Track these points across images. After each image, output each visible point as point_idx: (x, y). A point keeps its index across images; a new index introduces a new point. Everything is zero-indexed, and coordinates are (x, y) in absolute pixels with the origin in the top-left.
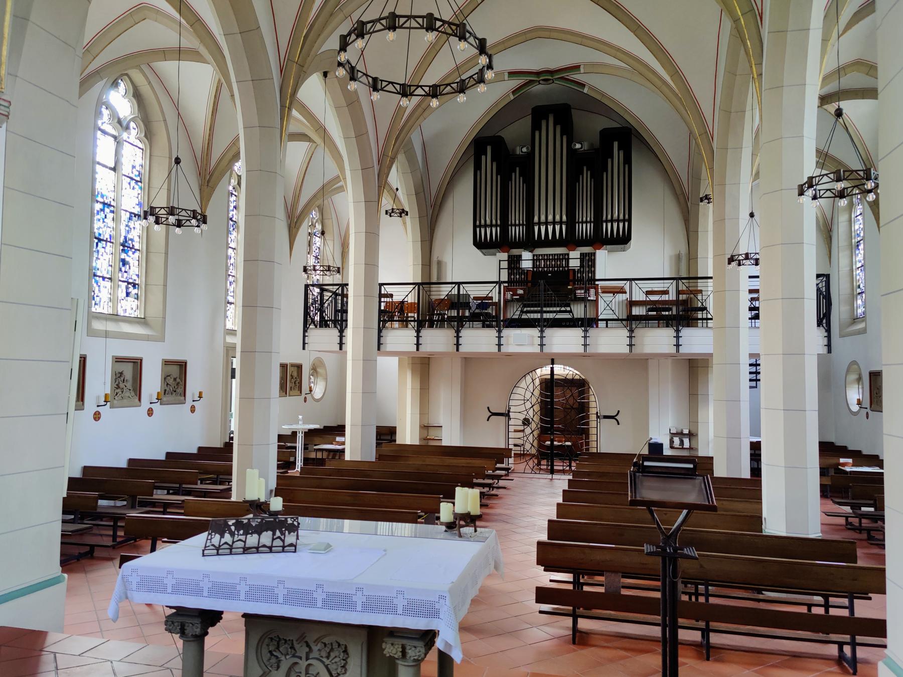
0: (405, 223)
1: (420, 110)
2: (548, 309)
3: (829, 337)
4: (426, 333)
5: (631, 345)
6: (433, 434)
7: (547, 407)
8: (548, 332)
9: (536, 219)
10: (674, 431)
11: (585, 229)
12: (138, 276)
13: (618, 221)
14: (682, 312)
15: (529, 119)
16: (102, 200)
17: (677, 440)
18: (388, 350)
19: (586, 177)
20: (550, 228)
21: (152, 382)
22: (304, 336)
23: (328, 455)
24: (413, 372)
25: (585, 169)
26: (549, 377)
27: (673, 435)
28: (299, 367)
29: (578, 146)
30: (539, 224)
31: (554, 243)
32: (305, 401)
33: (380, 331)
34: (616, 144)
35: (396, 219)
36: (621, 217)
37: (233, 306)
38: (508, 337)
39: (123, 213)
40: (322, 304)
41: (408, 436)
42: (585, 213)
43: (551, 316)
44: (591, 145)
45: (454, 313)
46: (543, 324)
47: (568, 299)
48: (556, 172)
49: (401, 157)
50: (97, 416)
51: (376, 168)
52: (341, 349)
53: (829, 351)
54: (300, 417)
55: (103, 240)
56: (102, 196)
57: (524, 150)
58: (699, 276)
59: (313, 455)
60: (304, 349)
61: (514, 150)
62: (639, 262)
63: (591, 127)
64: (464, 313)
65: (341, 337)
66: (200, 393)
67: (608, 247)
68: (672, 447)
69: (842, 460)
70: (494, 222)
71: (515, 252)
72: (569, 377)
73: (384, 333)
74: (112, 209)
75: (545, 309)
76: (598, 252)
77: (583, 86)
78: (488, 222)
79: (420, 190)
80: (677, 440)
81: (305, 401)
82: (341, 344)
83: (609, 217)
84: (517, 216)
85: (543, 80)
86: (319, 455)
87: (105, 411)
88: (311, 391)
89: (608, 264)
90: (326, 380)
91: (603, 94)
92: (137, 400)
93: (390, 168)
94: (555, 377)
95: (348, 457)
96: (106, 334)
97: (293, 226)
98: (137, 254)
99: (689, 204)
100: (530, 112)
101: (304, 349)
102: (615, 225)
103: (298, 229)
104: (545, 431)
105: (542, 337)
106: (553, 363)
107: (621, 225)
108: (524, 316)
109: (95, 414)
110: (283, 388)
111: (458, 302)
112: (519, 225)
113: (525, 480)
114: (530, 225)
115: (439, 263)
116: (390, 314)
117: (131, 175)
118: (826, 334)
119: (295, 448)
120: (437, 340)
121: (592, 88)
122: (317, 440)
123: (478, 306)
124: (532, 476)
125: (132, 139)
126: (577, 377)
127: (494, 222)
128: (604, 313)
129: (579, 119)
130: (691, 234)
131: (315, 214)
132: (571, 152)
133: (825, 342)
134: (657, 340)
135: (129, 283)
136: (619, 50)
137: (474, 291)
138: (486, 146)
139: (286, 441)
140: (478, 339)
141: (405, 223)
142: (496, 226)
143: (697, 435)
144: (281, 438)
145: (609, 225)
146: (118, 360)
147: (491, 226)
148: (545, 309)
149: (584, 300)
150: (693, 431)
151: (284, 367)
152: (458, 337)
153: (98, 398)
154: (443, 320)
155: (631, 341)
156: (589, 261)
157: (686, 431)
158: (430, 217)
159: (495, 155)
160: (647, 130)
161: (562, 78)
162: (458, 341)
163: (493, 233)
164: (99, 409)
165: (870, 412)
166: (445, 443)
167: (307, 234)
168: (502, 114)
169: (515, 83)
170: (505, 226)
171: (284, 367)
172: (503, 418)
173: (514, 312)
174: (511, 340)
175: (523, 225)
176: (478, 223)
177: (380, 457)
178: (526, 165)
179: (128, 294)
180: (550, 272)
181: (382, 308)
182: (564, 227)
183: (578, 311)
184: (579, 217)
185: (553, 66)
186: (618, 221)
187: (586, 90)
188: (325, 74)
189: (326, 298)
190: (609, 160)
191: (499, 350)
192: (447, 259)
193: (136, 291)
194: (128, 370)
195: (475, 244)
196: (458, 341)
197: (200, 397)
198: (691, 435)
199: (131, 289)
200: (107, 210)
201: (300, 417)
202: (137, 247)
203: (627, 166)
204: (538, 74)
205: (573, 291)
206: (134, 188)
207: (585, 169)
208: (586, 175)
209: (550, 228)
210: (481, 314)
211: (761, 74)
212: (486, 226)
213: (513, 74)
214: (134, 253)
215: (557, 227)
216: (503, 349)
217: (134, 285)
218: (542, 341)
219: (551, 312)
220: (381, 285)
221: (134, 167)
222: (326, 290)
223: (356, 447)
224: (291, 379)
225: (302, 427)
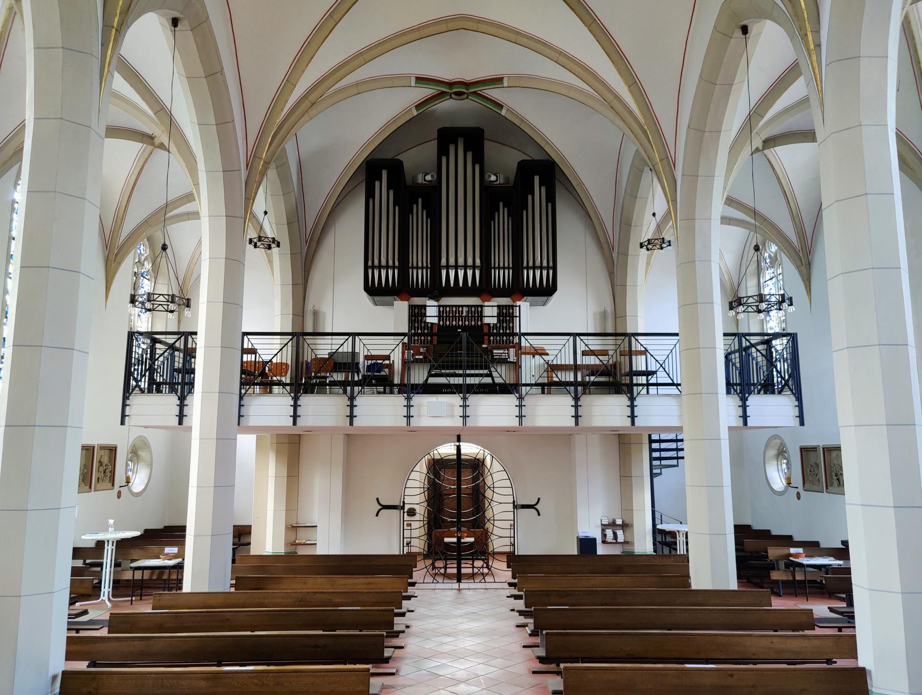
0: (270, 262)
1: (306, 104)
2: (472, 372)
3: (800, 407)
4: (306, 400)
5: (521, 417)
6: (303, 536)
7: (435, 495)
8: (473, 399)
10: (606, 522)
11: (501, 276)
14: (615, 377)
15: (435, 143)
17: (609, 532)
19: (503, 217)
20: (461, 273)
23: (152, 574)
24: (278, 453)
26: (455, 457)
27: (604, 527)
28: (112, 450)
30: (448, 267)
31: (465, 291)
32: (119, 497)
33: (241, 398)
34: (537, 179)
35: (261, 252)
38: (420, 406)
40: (153, 359)
41: (268, 541)
42: (502, 256)
43: (476, 381)
44: (507, 179)
45: (339, 377)
47: (486, 362)
48: (460, 213)
49: (272, 173)
51: (244, 174)
52: (180, 423)
53: (802, 423)
54: (111, 521)
57: (428, 178)
58: (639, 332)
59: (128, 575)
60: (122, 423)
61: (415, 178)
62: (557, 322)
63: (504, 162)
64: (353, 377)
65: (182, 406)
67: (529, 298)
68: (604, 542)
69: (793, 550)
70: (391, 263)
71: (417, 301)
73: (246, 400)
75: (468, 372)
77: (501, 106)
78: (384, 263)
79: (294, 218)
80: (609, 532)
81: (119, 497)
82: (181, 417)
83: (531, 264)
84: (419, 256)
85: (455, 93)
86: (138, 575)
88: (128, 482)
89: (530, 316)
90: (151, 465)
91: (522, 120)
93: (263, 174)
94: (462, 457)
95: (187, 587)
97: (112, 258)
99: (615, 255)
100: (435, 135)
101: (122, 423)
102: (538, 273)
103: (119, 264)
104: (435, 522)
105: (465, 406)
106: (459, 440)
108: (432, 380)
110: (86, 481)
111: (343, 363)
112: (422, 268)
114: (435, 267)
115: (316, 314)
116: (256, 377)
118: (797, 403)
119: (100, 565)
120: (323, 410)
121: (510, 110)
122: (135, 553)
123: (369, 368)
124: (432, 586)
128: (527, 376)
129: (490, 150)
130: (618, 289)
131: (143, 250)
132: (486, 188)
133: (796, 412)
134: (608, 411)
136: (561, 53)
137: (366, 348)
138: (379, 170)
139: (87, 558)
140: (379, 410)
141: (270, 262)
143: (632, 526)
144: (77, 552)
145: (531, 272)
148: (468, 372)
149: (504, 361)
150: (627, 522)
151: (88, 450)
152: (352, 406)
154: (325, 384)
156: (507, 315)
157: (619, 522)
158: (304, 256)
162: (632, 412)
165: (802, 493)
166: (322, 549)
167: (130, 274)
168: (403, 132)
169: (426, 92)
170: (404, 266)
171: (88, 450)
173: (419, 376)
174: (424, 410)
176: (370, 263)
177: (240, 583)
178: (430, 197)
180: (459, 327)
183: (501, 374)
185: (469, 77)
186: (541, 268)
187: (503, 112)
188: (175, 22)
189: (159, 352)
190: (530, 197)
192: (326, 308)
195: (365, 290)
196: (632, 412)
198: (625, 526)
201: (111, 521)
203: (550, 205)
204: (451, 84)
205: (489, 352)
209: (461, 273)
210: (374, 377)
211: (820, 45)
212: (380, 267)
213: (421, 80)
215: (470, 273)
216: (414, 422)
218: (465, 411)
219: (477, 375)
220: (246, 334)
222: (160, 342)
223: (201, 570)
224: (99, 467)
225: (112, 535)
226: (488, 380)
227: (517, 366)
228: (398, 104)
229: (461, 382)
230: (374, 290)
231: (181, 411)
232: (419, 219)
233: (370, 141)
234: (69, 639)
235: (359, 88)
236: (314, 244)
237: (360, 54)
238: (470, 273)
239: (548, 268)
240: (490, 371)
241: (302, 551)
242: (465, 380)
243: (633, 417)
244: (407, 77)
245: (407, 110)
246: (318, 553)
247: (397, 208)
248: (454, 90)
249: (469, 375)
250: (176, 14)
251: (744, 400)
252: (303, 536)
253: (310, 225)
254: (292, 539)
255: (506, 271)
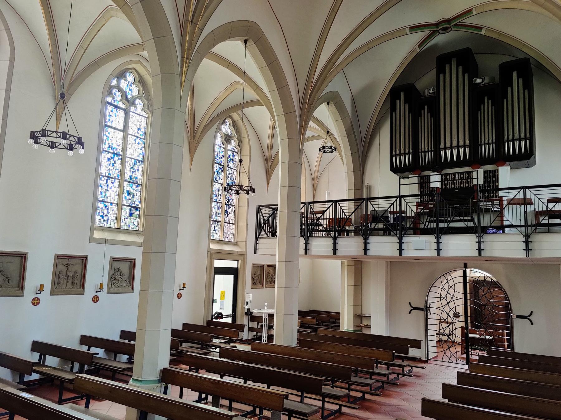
9: (442, 146)
11: (487, 150)
12: (140, 202)
13: (520, 140)
16: (112, 151)
18: (313, 254)
19: (487, 107)
21: (97, 274)
22: (256, 244)
25: (486, 98)
29: (478, 81)
30: (445, 149)
31: (459, 163)
34: (515, 74)
36: (523, 135)
37: (220, 223)
39: (127, 160)
42: (487, 135)
46: (439, 233)
50: (95, 299)
55: (112, 178)
56: (113, 149)
57: (431, 91)
60: (255, 253)
66: (184, 284)
67: (511, 163)
71: (425, 173)
72: (481, 279)
74: (120, 157)
76: (500, 168)
77: (480, 28)
79: (352, 132)
84: (426, 144)
85: (442, 29)
87: (102, 295)
91: (500, 33)
92: (130, 288)
95: (274, 343)
96: (106, 242)
98: (139, 188)
101: (255, 253)
102: (517, 144)
106: (466, 266)
107: (523, 143)
109: (178, 294)
113: (442, 368)
114: (437, 151)
115: (369, 188)
117: (137, 135)
120: (383, 246)
121: (489, 29)
125: (139, 111)
126: (488, 279)
127: (407, 151)
132: (473, 87)
135: (132, 207)
142: (409, 153)
146: (114, 260)
147: (405, 154)
149: (489, 211)
153: (180, 285)
155: (527, 246)
156: (492, 177)
159: (410, 100)
160: (547, 59)
161: (456, 25)
163: (406, 160)
164: (181, 292)
166: (374, 331)
168: (414, 65)
169: (419, 36)
170: (416, 152)
172: (421, 313)
175: (492, 143)
176: (394, 153)
178: (433, 104)
179: (131, 215)
180: (457, 188)
181: (303, 222)
182: (467, 150)
184: (482, 139)
185: (449, 15)
186: (520, 140)
187: (483, 32)
188: (246, 42)
190: (509, 89)
191: (401, 254)
193: (138, 212)
194: (125, 268)
195: (391, 170)
197: (184, 287)
199: (134, 211)
200: (116, 158)
201: (266, 304)
202: (140, 182)
203: (526, 91)
204: (437, 24)
206: (138, 143)
207: (486, 98)
208: (487, 104)
209: (455, 152)
212: (400, 154)
213: (414, 28)
214: (137, 187)
215: (461, 150)
217: (137, 208)
221: (139, 129)
226: (470, 224)
227: (500, 214)
228: (404, 48)
229: (435, 226)
230: (394, 169)
231: (366, 246)
232: (426, 119)
233: (393, 76)
234: (170, 360)
235: (369, 46)
236: (367, 145)
237: (360, 26)
238: (461, 150)
239: (525, 139)
240: (472, 217)
241: (365, 331)
242: (438, 225)
243: (401, 250)
244: (404, 29)
245: (414, 49)
246: (372, 333)
247: (410, 115)
248: (440, 28)
249: (441, 222)
250: (246, 38)
251: (366, 239)
252: (365, 322)
253: (363, 134)
254: (358, 323)
255: (491, 146)
